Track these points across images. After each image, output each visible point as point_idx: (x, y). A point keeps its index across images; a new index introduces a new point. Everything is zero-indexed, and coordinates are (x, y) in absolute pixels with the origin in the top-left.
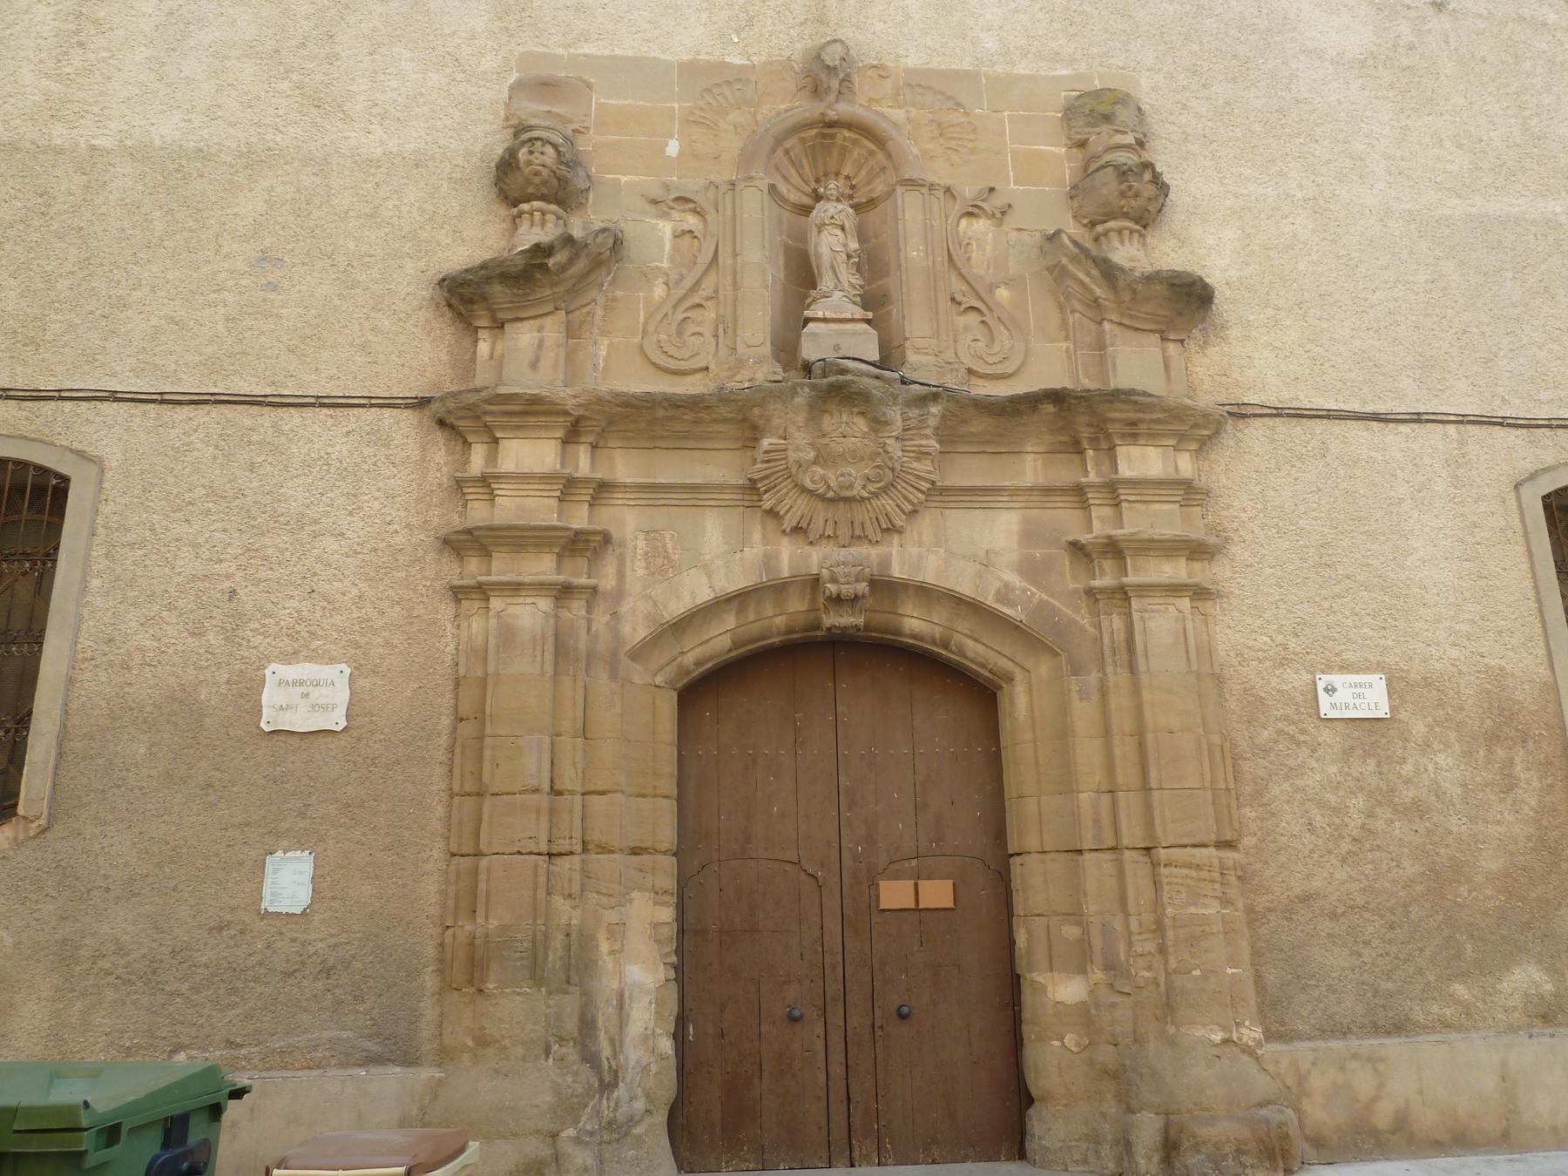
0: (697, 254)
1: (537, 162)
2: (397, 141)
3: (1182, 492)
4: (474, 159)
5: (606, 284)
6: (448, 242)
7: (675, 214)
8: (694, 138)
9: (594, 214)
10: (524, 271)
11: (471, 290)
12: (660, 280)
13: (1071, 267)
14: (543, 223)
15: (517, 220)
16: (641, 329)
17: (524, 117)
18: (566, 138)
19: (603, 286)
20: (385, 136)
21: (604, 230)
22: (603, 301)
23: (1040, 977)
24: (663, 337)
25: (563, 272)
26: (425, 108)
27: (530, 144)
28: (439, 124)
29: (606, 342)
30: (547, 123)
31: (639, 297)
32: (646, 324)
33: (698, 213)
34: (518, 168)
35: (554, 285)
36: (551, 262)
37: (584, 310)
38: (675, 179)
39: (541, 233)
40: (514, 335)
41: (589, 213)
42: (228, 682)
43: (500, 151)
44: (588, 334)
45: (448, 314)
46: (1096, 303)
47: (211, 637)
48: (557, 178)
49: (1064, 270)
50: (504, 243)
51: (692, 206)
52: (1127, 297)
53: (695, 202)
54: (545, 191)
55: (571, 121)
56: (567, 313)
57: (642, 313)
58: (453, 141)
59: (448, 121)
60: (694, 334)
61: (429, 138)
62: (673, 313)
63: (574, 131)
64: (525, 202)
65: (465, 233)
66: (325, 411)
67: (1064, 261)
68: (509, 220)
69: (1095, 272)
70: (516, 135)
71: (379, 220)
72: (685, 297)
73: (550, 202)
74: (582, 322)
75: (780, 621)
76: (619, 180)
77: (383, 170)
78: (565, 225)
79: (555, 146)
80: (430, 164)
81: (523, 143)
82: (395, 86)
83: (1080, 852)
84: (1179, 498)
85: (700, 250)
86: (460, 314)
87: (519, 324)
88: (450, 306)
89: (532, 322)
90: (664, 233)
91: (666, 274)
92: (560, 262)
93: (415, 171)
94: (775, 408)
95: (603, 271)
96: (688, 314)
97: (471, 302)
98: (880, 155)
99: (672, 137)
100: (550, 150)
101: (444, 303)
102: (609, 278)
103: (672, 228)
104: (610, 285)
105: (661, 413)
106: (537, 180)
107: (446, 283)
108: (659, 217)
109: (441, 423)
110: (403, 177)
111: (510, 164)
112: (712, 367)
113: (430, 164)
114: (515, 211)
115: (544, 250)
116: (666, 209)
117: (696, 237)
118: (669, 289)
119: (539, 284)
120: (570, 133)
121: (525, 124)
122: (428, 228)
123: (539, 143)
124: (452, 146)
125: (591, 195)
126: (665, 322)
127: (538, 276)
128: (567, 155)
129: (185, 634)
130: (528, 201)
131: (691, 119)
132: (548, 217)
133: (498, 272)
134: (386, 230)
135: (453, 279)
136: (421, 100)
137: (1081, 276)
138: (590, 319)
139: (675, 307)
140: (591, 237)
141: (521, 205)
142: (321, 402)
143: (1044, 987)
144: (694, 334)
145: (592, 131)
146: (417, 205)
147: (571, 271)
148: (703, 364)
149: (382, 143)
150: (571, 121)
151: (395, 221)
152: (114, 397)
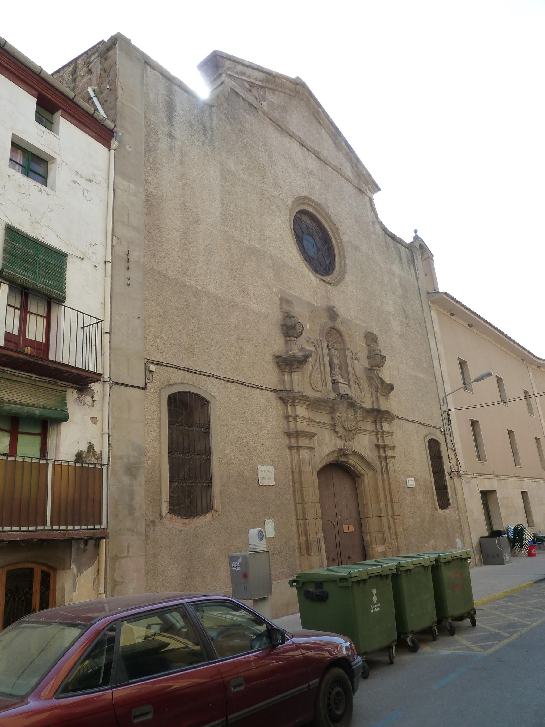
3: (308, 421)
13: (375, 378)
23: (374, 546)
34: (296, 329)
42: (250, 470)
46: (377, 388)
47: (245, 456)
49: (373, 378)
52: (383, 388)
66: (258, 390)
67: (374, 376)
69: (380, 381)
75: (332, 459)
83: (381, 517)
84: (307, 422)
94: (340, 406)
98: (340, 339)
105: (321, 403)
109: (281, 398)
112: (322, 391)
129: (239, 455)
137: (376, 381)
142: (256, 387)
143: (375, 548)
148: (320, 390)
152: (213, 376)
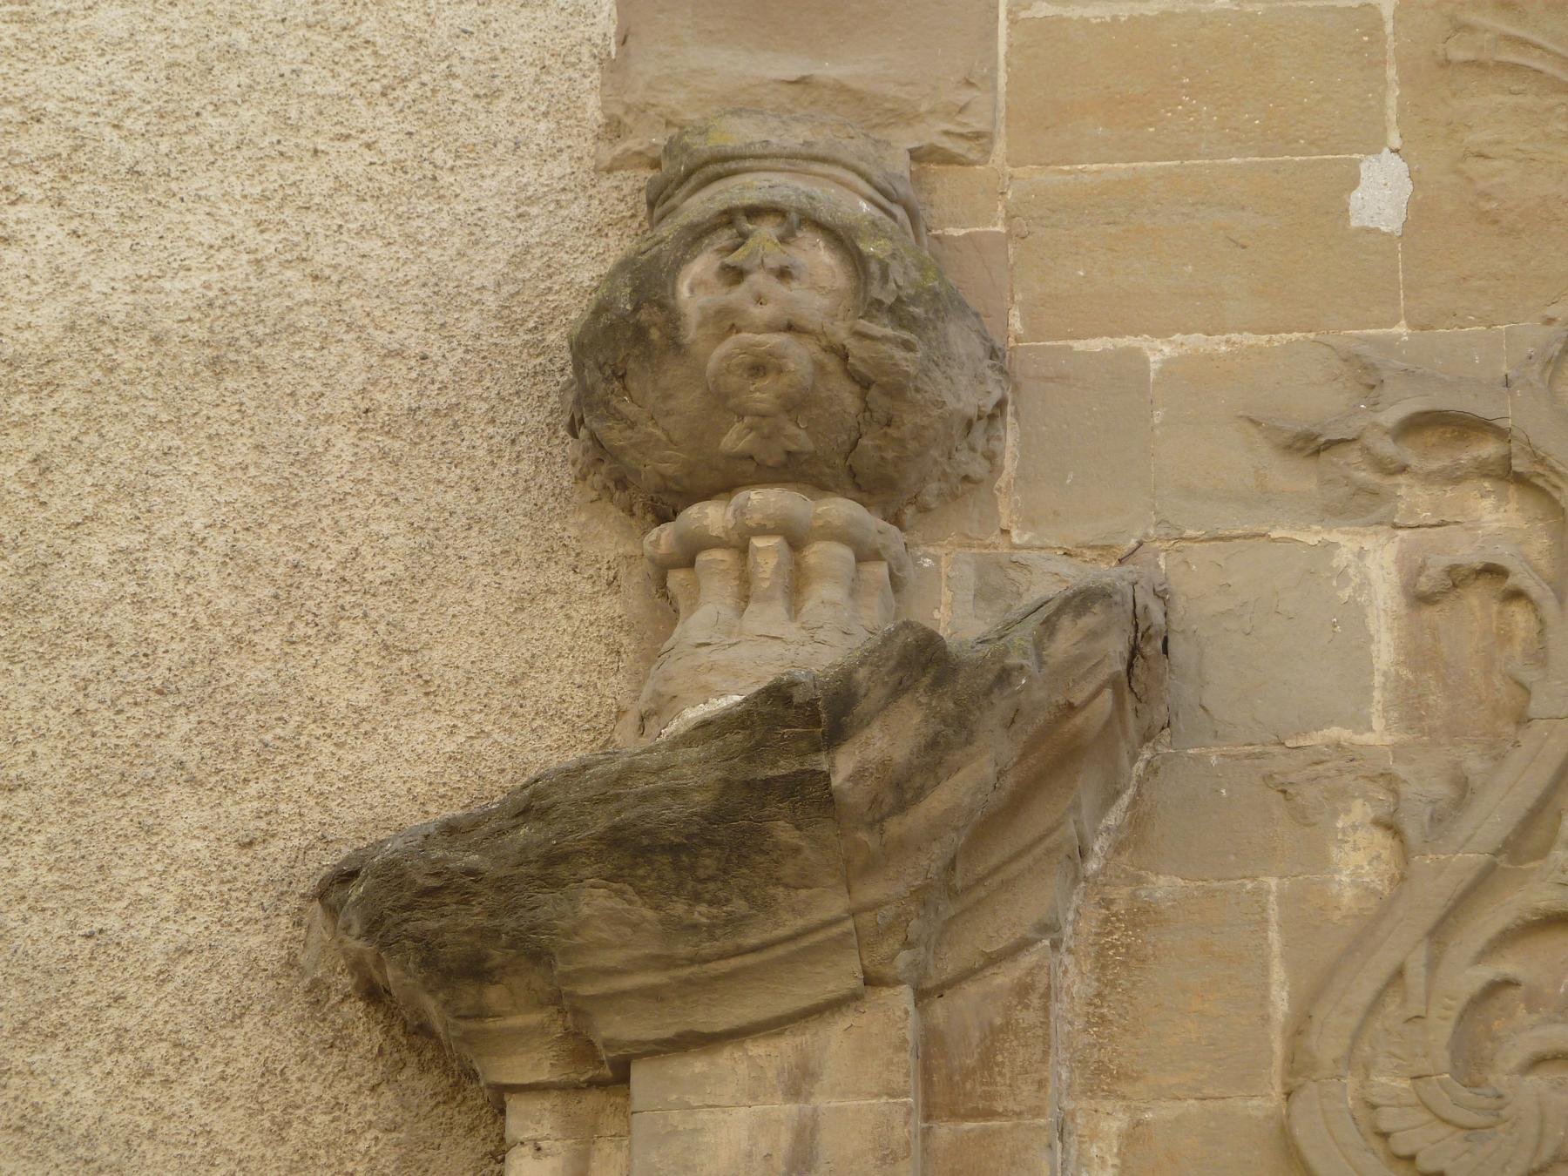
0: (1529, 675)
1: (760, 313)
2: (125, 268)
4: (472, 320)
5: (1099, 845)
6: (362, 698)
7: (1412, 496)
8: (1479, 137)
9: (1030, 522)
10: (719, 815)
11: (474, 917)
12: (1360, 811)
14: (796, 585)
15: (676, 578)
16: (1278, 1047)
17: (691, 116)
18: (886, 195)
19: (1083, 853)
20: (77, 251)
21: (1082, 600)
22: (1089, 926)
24: (1389, 1083)
25: (901, 807)
26: (246, 114)
27: (724, 237)
28: (316, 181)
29: (1114, 1123)
30: (796, 136)
31: (1260, 893)
32: (1298, 1030)
33: (1521, 480)
34: (675, 346)
35: (853, 872)
36: (843, 766)
37: (1004, 978)
38: (1401, 330)
39: (791, 630)
40: (676, 1117)
41: (1005, 515)
43: (588, 274)
44: (1027, 1091)
45: (368, 1034)
48: (852, 376)
50: (616, 687)
51: (1489, 449)
53: (1502, 434)
54: (798, 437)
55: (902, 116)
56: (923, 996)
57: (1278, 973)
58: (373, 245)
59: (351, 163)
60: (1538, 1062)
61: (269, 244)
62: (1433, 965)
63: (916, 155)
64: (708, 495)
65: (437, 654)
68: (635, 580)
70: (659, 199)
71: (47, 623)
72: (1483, 882)
73: (821, 486)
74: (994, 1037)
76: (1135, 355)
77: (70, 399)
78: (896, 583)
79: (840, 238)
80: (274, 354)
81: (697, 235)
82: (120, 30)
85: (1539, 656)
86: (423, 1030)
87: (697, 1065)
88: (373, 994)
89: (757, 1049)
90: (1366, 583)
91: (1389, 780)
92: (884, 764)
93: (209, 394)
95: (1087, 783)
96: (1508, 966)
97: (477, 971)
99: (1374, 145)
100: (818, 257)
101: (346, 981)
102: (1113, 818)
103: (1401, 561)
104: (1118, 848)
106: (763, 394)
107: (356, 891)
108: (1335, 513)
110: (154, 422)
111: (640, 333)
113: (274, 354)
114: (663, 538)
115: (809, 715)
116: (1365, 476)
117: (1517, 595)
118: (1405, 852)
119: (788, 870)
120: (900, 165)
121: (703, 146)
122: (271, 641)
123: (766, 231)
124: (372, 270)
125: (1010, 437)
126: (1392, 1006)
127: (784, 832)
128: (896, 273)
130: (724, 488)
131: (1459, 54)
132: (819, 554)
133: (601, 822)
134: (83, 667)
135: (392, 873)
136: (233, 81)
138: (1028, 1017)
139: (1439, 933)
140: (1022, 636)
141: (693, 511)
144: (1538, 1062)
145: (1000, 147)
146: (219, 541)
147: (942, 799)
149: (62, 278)
150: (902, 116)
151: (121, 619)
